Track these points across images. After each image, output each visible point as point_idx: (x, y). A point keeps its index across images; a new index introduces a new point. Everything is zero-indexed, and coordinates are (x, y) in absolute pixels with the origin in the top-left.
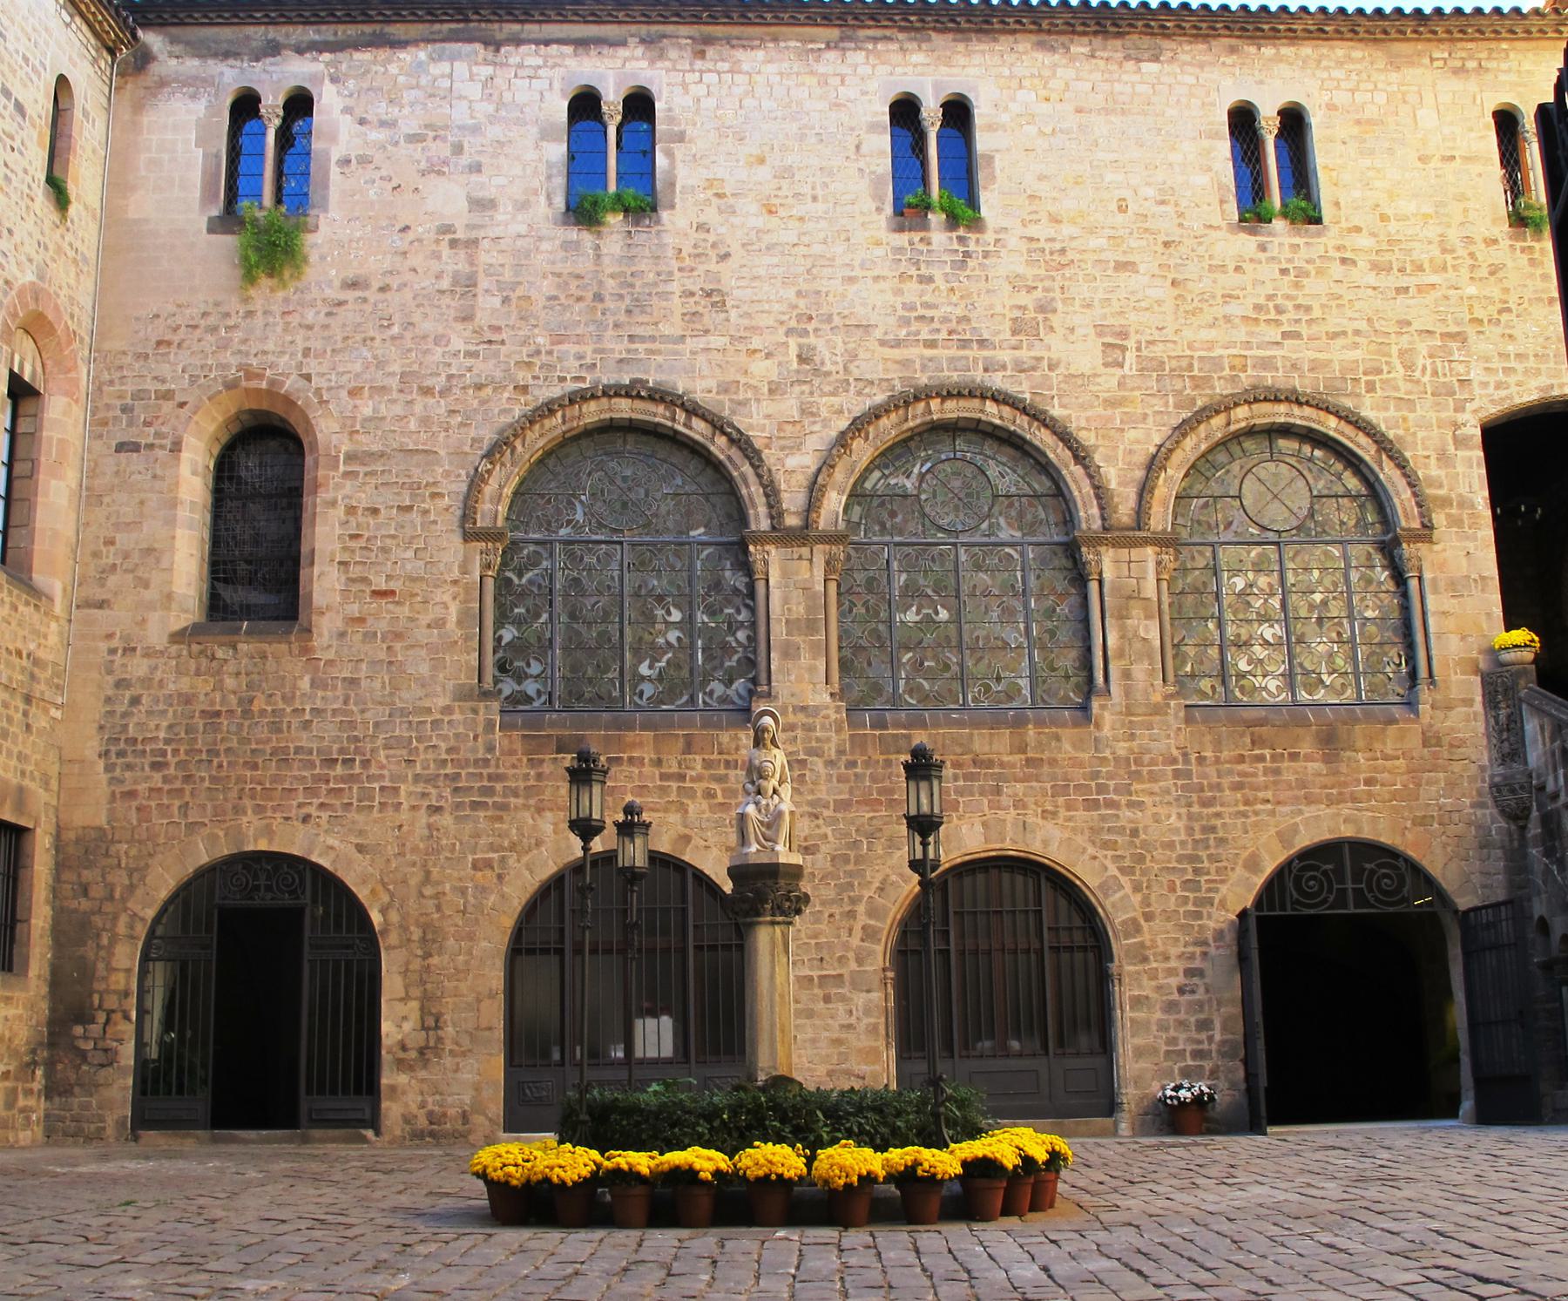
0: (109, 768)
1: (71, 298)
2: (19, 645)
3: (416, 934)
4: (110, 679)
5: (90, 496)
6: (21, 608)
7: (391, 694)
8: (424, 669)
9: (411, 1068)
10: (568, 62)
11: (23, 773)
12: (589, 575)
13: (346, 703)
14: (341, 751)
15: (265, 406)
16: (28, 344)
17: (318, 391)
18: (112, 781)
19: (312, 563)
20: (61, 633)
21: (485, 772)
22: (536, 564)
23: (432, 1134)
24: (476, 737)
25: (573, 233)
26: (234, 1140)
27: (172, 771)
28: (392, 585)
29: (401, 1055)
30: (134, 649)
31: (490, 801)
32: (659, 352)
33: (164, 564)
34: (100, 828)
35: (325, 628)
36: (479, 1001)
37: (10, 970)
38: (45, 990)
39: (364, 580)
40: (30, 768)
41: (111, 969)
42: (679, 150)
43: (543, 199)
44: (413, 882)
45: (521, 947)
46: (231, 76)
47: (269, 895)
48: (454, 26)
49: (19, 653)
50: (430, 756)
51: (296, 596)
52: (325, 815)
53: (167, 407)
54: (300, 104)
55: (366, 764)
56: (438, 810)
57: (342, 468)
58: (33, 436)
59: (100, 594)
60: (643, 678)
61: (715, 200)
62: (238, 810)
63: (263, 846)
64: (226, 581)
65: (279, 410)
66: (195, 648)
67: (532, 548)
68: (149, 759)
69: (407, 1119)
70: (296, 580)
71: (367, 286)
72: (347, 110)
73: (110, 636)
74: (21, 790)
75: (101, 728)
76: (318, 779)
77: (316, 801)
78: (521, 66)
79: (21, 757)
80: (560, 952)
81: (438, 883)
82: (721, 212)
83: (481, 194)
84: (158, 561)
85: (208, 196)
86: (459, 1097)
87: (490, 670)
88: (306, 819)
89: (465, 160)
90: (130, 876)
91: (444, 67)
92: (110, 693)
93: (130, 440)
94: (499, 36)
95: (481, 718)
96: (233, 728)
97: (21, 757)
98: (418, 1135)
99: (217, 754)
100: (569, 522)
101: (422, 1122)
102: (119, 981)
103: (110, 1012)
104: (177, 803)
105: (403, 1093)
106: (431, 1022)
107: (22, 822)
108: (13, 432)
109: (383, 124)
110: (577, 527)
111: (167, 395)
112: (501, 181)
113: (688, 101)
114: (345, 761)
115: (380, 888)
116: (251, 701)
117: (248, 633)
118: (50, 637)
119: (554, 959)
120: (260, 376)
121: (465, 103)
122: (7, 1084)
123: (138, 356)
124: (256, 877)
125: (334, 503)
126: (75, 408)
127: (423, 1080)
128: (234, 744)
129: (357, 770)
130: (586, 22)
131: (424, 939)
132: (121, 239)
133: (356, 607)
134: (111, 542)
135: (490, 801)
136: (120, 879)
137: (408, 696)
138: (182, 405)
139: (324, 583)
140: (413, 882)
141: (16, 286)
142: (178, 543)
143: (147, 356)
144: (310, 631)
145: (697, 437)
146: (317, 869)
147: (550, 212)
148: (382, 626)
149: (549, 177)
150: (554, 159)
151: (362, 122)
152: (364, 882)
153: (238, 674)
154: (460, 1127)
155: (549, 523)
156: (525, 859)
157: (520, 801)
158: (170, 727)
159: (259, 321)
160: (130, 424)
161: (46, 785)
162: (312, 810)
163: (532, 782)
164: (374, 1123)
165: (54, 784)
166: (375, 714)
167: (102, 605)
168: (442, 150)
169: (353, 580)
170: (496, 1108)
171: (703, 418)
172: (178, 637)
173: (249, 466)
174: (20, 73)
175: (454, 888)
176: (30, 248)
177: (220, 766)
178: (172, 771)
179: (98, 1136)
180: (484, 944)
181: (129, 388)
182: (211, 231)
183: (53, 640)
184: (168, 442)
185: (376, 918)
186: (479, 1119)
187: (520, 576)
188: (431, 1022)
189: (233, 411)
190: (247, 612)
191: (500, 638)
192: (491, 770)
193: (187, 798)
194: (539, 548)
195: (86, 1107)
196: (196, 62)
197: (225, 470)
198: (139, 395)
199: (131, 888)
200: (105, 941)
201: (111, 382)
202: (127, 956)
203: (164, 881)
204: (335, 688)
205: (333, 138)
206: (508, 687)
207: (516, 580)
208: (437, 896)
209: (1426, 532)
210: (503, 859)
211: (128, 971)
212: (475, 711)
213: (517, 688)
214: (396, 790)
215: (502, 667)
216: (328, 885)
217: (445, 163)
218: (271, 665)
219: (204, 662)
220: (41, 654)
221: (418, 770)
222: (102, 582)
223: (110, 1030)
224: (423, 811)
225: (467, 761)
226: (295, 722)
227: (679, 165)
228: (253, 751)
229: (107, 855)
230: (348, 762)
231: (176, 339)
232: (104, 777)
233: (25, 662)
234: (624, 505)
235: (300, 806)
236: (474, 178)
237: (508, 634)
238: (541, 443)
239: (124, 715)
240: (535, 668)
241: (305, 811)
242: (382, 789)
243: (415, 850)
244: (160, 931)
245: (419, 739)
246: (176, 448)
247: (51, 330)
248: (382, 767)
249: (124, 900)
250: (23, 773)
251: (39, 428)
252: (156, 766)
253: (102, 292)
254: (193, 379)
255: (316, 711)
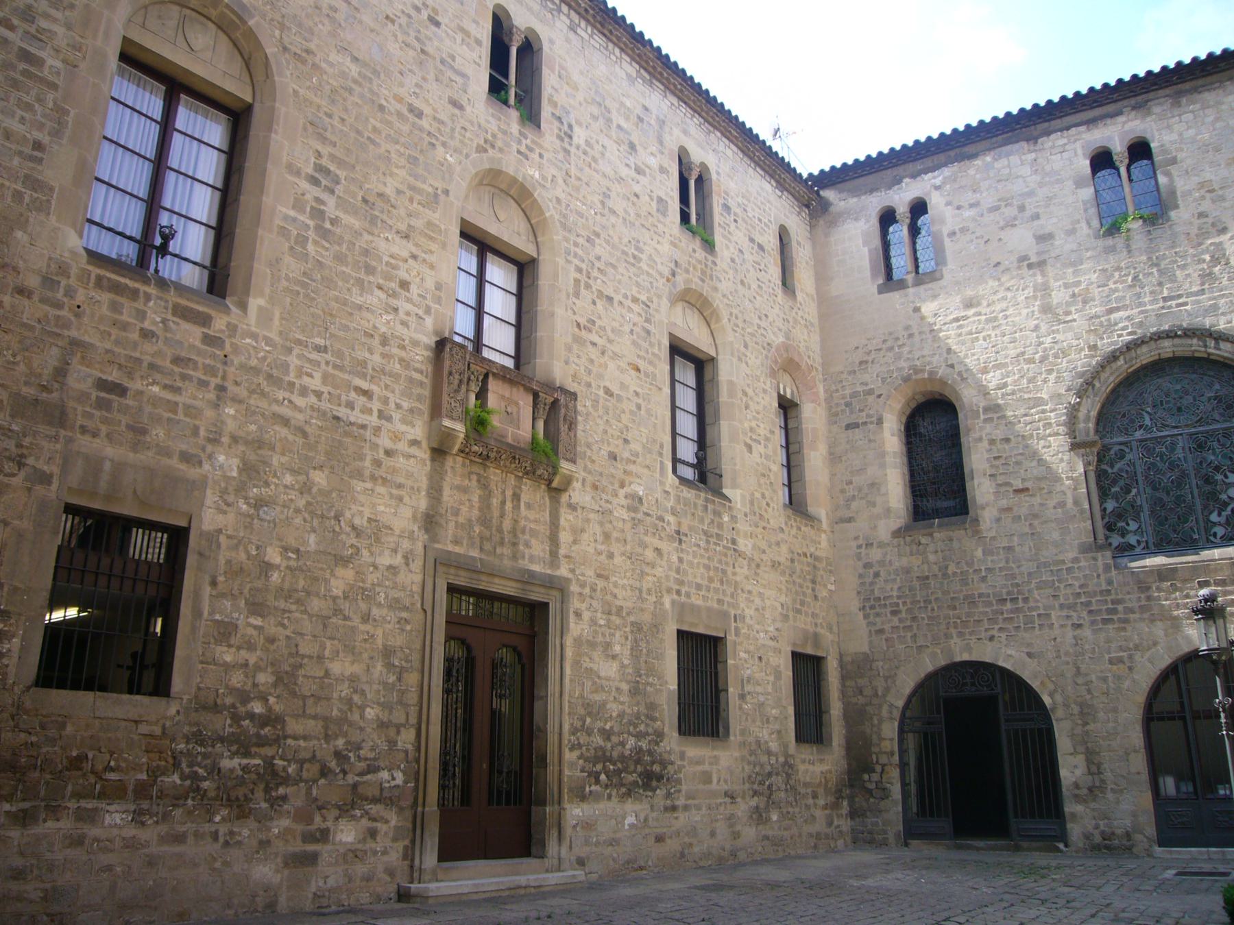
0: (866, 617)
1: (807, 348)
2: (805, 550)
3: (1076, 710)
4: (860, 564)
5: (834, 458)
6: (803, 528)
7: (1036, 554)
8: (1056, 535)
9: (1085, 801)
10: (1084, 136)
11: (816, 625)
12: (1162, 459)
13: (1007, 562)
14: (1008, 593)
15: (929, 388)
16: (787, 377)
17: (960, 374)
18: (869, 624)
19: (973, 478)
20: (829, 540)
21: (1109, 598)
22: (1122, 457)
23: (1107, 847)
24: (1099, 576)
25: (1110, 241)
26: (969, 847)
27: (903, 615)
28: (1027, 485)
29: (1077, 792)
30: (872, 544)
31: (1115, 617)
32: (1186, 304)
33: (883, 490)
34: (865, 653)
35: (987, 517)
36: (1127, 754)
37: (822, 742)
38: (843, 753)
39: (1008, 484)
40: (820, 621)
41: (881, 739)
42: (1174, 170)
43: (1084, 225)
44: (1069, 675)
45: (1151, 716)
46: (874, 203)
47: (974, 688)
48: (1005, 136)
49: (805, 555)
50: (1069, 591)
51: (965, 500)
52: (1003, 635)
53: (871, 399)
54: (919, 208)
55: (1026, 600)
56: (1079, 626)
57: (982, 417)
58: (798, 429)
59: (848, 514)
60: (1214, 524)
61: (1208, 195)
62: (948, 636)
63: (966, 657)
64: (921, 496)
65: (937, 388)
66: (908, 539)
67: (1117, 448)
68: (889, 609)
69: (1087, 836)
70: (964, 490)
71: (979, 304)
72: (948, 204)
73: (857, 538)
74: (816, 635)
75: (859, 593)
76: (996, 612)
77: (997, 627)
78: (1053, 147)
79: (814, 615)
80: (1183, 719)
81: (1087, 675)
82: (1213, 201)
83: (1041, 232)
84: (879, 490)
85: (874, 276)
86: (1122, 823)
87: (1101, 532)
88: (992, 638)
89: (1028, 213)
90: (886, 681)
91: (1004, 162)
92: (861, 571)
93: (852, 420)
94: (1035, 133)
95: (1100, 563)
96: (938, 586)
97: (814, 615)
98: (1096, 848)
99: (930, 602)
100: (1141, 427)
101: (1098, 839)
102: (886, 746)
103: (883, 766)
104: (909, 634)
105: (1081, 818)
106: (1094, 765)
107: (819, 654)
108: (786, 429)
109: (971, 206)
110: (1148, 429)
111: (870, 392)
112: (1055, 220)
113: (1175, 137)
114: (1012, 600)
115: (1047, 680)
116: (946, 568)
117: (940, 526)
118: (823, 544)
119: (1179, 723)
120: (922, 371)
121: (1020, 180)
122: (827, 812)
123: (850, 373)
124: (964, 678)
125: (980, 439)
126: (819, 409)
127: (1093, 810)
128: (940, 595)
129: (1021, 604)
130: (1092, 108)
131: (1081, 713)
132: (829, 308)
133: (1005, 502)
134: (850, 483)
135: (1115, 617)
136: (880, 684)
137: (1047, 554)
138: (879, 396)
139: (981, 489)
140: (1069, 675)
141: (774, 345)
142: (889, 478)
143: (855, 372)
144: (977, 520)
145: (1226, 355)
146: (1003, 671)
147: (1091, 232)
148: (1023, 511)
149: (1086, 210)
150: (1086, 198)
151: (959, 208)
152: (1036, 677)
153: (936, 552)
154: (1125, 842)
155: (1126, 429)
156: (1148, 654)
157: (1137, 616)
158: (899, 588)
159: (917, 338)
160: (851, 413)
161: (830, 629)
162: (995, 633)
163: (1143, 603)
164: (1063, 837)
165: (835, 629)
166: (1028, 567)
167: (850, 520)
168: (1010, 212)
169: (1000, 485)
170: (1151, 831)
171: (1227, 340)
172: (897, 533)
173: (925, 426)
174: (758, 228)
175: (1099, 678)
176: (779, 323)
177: (933, 610)
178: (903, 615)
179: (884, 843)
180: (1126, 715)
181: (847, 392)
182: (880, 292)
183: (824, 544)
184: (874, 419)
185: (1047, 700)
186: (1138, 837)
187: (1112, 467)
188: (1094, 769)
189: (910, 394)
190: (937, 513)
191: (1105, 509)
192: (1113, 597)
193: (915, 631)
194: (1122, 447)
195: (876, 824)
196: (855, 200)
197: (911, 430)
198: (854, 395)
199: (887, 689)
200: (876, 722)
201: (837, 391)
202: (890, 730)
203: (907, 683)
204: (998, 554)
205: (942, 221)
206: (1116, 540)
207: (1110, 471)
208: (1086, 684)
209: (638, 72)
210: (1130, 657)
211: (892, 740)
212: (1095, 559)
213: (1122, 540)
214: (1048, 616)
215: (1109, 528)
216: (932, 677)
217: (1015, 219)
218: (955, 544)
219: (915, 547)
220: (818, 553)
221: (1062, 600)
222: (848, 507)
223: (884, 777)
224: (1069, 628)
225: (1095, 592)
226: (976, 578)
227: (1176, 179)
228: (952, 599)
229: (871, 669)
230: (1014, 600)
231: (870, 359)
232: (863, 623)
233: (809, 560)
234: (1179, 409)
235: (986, 630)
236: (1036, 223)
237: (1110, 505)
238: (1112, 379)
239: (872, 584)
240: (1133, 526)
241: (991, 633)
242: (1039, 615)
243: (1067, 654)
244: (908, 714)
245: (1059, 581)
246: (880, 421)
247: (798, 366)
248: (1037, 601)
249: (884, 696)
250: (816, 625)
251: (800, 423)
252: (894, 613)
253: (823, 341)
254: (884, 380)
255: (989, 570)
